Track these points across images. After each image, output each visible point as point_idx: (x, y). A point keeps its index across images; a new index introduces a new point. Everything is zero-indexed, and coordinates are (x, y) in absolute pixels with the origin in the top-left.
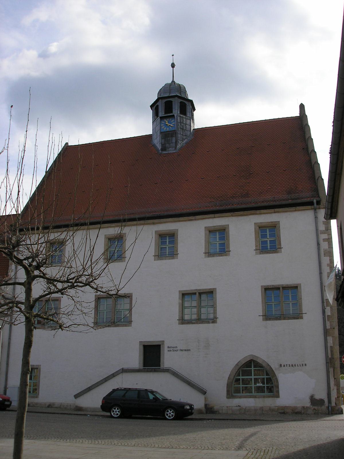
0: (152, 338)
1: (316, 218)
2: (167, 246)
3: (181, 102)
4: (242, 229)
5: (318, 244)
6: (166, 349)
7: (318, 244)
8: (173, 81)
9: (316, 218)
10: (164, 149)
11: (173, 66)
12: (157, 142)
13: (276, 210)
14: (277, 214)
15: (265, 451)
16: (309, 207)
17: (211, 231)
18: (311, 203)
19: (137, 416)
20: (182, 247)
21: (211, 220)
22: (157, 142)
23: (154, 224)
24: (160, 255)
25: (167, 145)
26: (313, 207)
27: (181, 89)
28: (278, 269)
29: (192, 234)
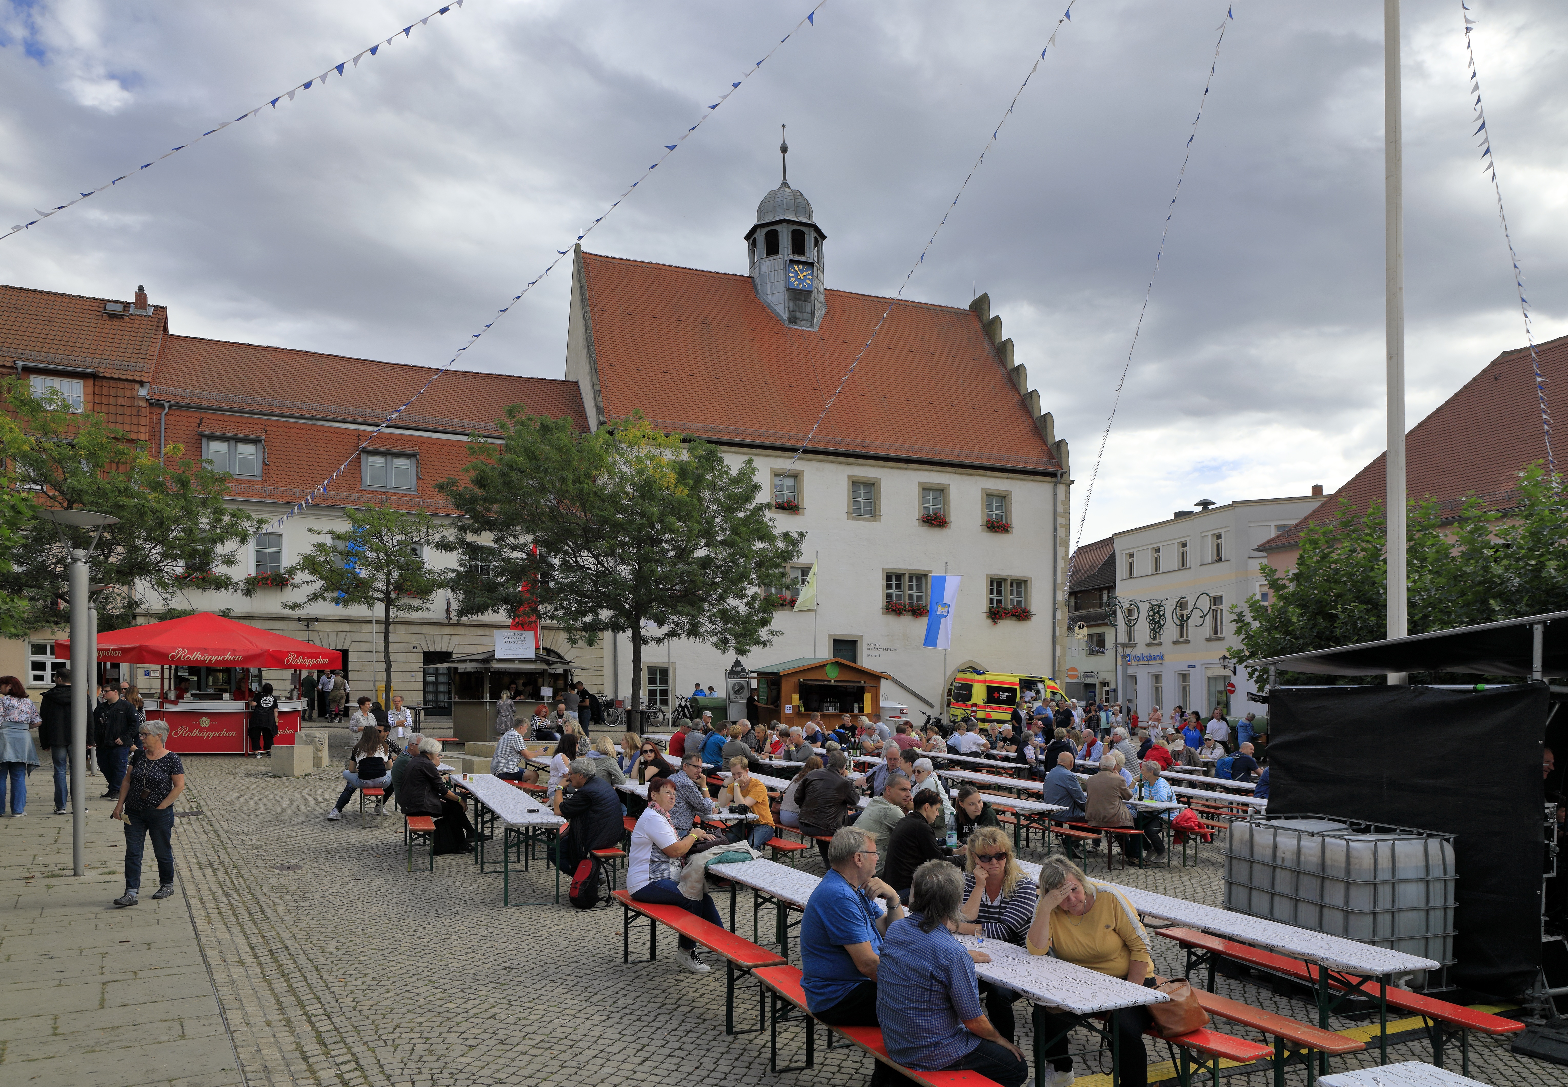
0: (845, 631)
1: (1055, 495)
2: (865, 502)
3: (794, 232)
4: (966, 495)
5: (1055, 530)
6: (865, 647)
7: (1055, 530)
8: (785, 185)
9: (1055, 495)
10: (793, 320)
11: (784, 149)
12: (777, 301)
13: (1011, 475)
14: (1009, 481)
15: (282, 868)
16: (1049, 479)
17: (926, 489)
18: (1053, 475)
19: (8, 796)
20: (886, 504)
21: (926, 473)
22: (777, 301)
23: (847, 464)
24: (855, 512)
25: (798, 314)
26: (1054, 479)
27: (801, 204)
28: (918, 551)
29: (900, 489)
